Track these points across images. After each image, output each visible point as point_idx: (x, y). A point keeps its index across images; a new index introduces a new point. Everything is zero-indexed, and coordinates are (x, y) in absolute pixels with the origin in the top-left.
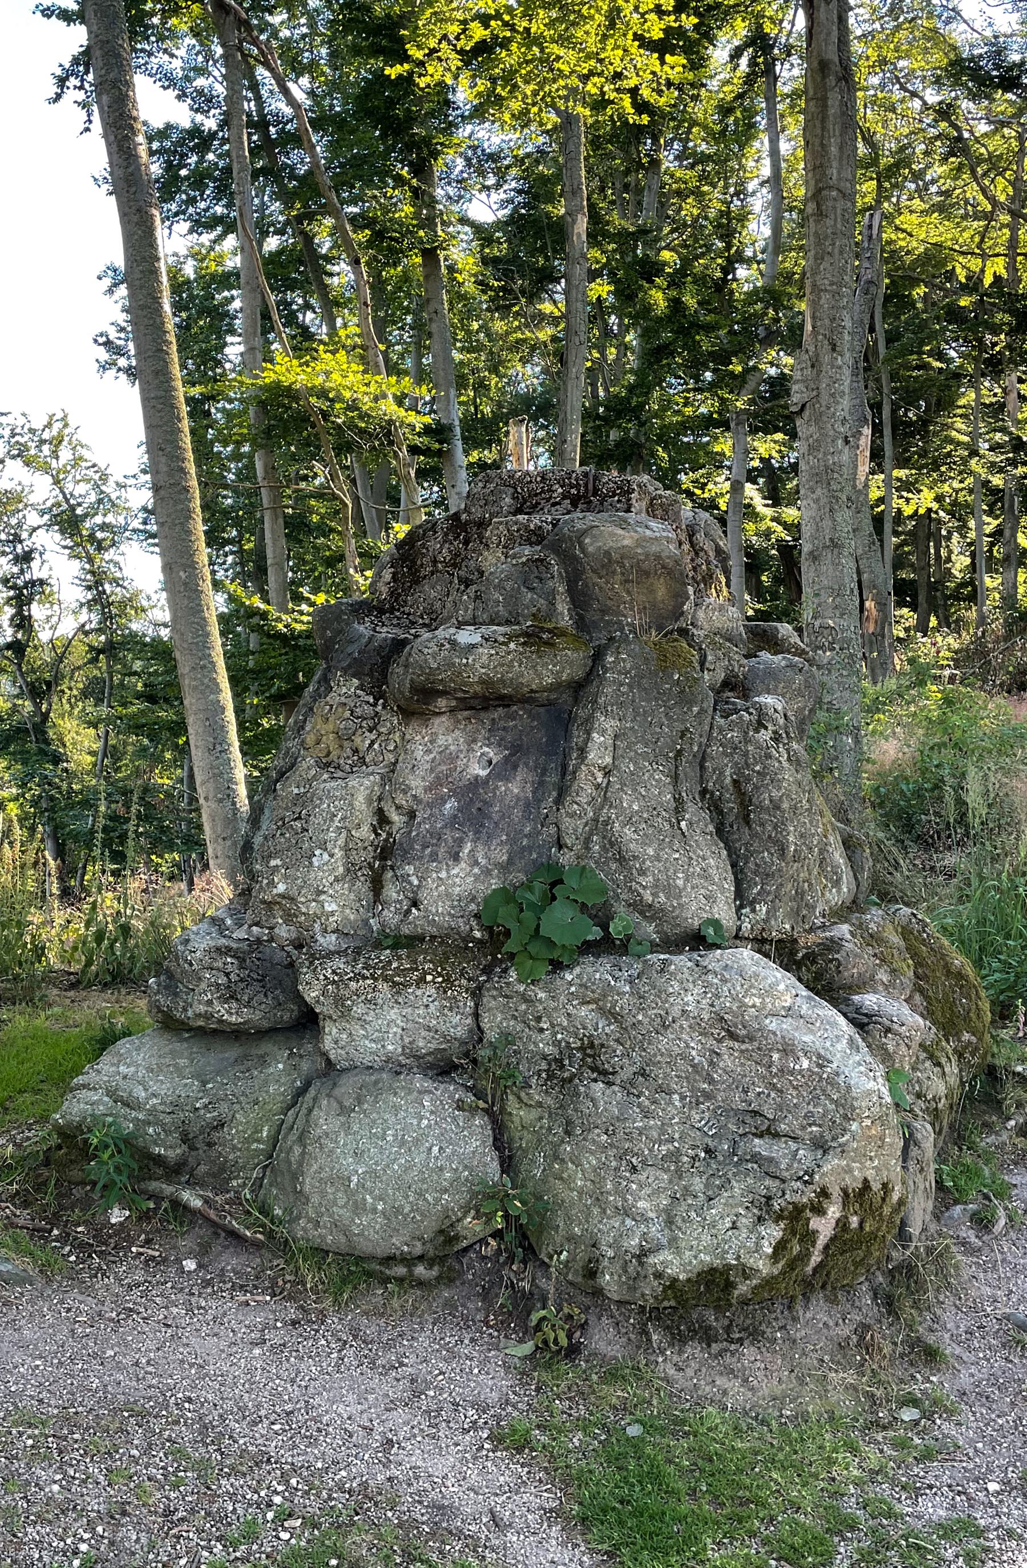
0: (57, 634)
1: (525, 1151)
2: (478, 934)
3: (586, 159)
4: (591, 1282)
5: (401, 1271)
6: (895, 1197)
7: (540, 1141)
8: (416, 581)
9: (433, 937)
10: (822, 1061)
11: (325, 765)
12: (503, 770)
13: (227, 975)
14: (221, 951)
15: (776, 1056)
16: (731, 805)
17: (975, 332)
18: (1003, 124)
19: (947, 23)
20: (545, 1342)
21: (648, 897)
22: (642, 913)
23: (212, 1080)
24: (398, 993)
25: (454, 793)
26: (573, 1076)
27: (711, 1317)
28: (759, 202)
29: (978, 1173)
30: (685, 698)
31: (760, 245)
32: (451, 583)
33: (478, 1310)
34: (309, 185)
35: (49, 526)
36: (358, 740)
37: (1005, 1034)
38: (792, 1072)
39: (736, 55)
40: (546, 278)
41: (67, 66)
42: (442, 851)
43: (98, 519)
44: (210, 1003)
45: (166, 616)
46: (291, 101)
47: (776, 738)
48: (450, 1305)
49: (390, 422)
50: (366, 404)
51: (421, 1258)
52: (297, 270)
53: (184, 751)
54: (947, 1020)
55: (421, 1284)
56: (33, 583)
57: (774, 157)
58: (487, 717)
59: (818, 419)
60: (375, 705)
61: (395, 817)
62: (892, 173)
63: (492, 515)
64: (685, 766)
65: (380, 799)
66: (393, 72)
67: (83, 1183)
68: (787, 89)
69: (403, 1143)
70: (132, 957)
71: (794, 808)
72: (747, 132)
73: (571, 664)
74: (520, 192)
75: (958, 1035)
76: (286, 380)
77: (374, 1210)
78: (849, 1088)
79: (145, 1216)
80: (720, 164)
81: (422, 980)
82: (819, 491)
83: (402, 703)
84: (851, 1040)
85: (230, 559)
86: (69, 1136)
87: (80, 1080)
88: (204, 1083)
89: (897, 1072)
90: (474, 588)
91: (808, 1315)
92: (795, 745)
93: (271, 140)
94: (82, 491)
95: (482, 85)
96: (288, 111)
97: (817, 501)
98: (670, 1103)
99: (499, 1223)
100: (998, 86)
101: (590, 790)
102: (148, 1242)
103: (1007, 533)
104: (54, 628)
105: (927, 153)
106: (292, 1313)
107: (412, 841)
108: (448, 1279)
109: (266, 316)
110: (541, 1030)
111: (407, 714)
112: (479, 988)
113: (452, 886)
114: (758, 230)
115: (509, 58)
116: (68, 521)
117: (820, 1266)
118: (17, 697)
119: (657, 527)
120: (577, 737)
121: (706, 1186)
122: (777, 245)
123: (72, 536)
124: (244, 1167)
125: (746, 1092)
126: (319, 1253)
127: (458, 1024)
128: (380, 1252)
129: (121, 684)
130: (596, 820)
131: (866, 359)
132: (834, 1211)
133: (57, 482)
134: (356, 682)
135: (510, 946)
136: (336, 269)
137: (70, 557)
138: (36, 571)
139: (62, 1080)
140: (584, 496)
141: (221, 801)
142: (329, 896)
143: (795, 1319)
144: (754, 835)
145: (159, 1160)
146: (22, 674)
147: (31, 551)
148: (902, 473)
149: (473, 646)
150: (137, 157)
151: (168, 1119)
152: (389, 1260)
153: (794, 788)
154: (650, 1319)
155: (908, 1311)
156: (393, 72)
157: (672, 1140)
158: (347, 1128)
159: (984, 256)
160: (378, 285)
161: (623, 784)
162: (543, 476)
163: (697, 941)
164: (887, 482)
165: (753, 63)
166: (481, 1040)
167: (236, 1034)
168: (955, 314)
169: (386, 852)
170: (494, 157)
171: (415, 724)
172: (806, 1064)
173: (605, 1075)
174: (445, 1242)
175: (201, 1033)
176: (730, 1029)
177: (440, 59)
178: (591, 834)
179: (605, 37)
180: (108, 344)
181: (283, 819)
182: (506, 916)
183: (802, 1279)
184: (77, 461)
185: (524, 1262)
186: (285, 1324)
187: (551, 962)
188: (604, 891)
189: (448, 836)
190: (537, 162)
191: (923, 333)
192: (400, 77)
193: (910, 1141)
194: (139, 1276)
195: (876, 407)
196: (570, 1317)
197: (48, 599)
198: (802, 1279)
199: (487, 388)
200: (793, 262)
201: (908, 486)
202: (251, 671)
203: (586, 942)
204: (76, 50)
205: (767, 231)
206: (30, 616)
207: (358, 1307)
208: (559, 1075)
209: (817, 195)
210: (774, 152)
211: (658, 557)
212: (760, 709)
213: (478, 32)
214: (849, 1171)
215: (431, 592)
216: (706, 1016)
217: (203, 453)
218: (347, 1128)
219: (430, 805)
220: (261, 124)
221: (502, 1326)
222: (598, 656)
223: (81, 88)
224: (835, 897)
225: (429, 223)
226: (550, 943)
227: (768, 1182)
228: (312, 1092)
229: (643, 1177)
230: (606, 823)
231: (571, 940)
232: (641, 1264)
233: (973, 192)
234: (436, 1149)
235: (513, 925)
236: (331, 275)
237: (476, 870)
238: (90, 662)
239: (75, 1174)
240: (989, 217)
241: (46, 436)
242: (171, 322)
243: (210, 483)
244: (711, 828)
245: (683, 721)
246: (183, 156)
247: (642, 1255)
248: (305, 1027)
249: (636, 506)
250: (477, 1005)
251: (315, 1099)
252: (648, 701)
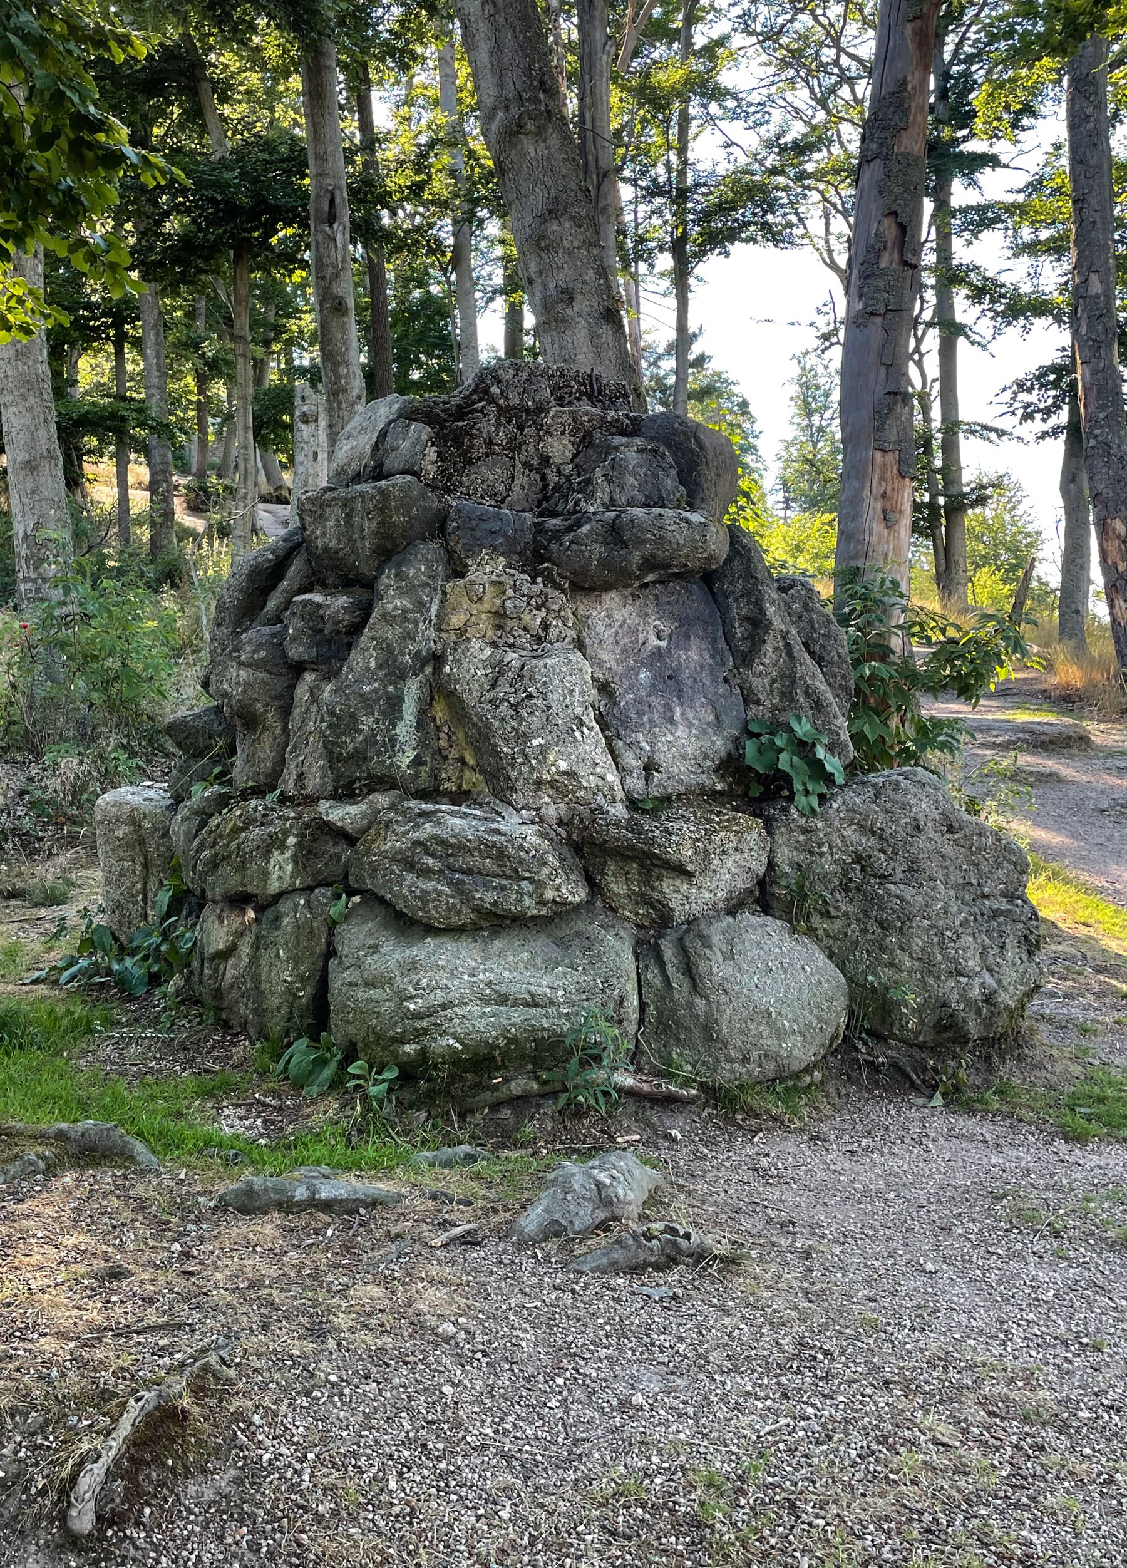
32: (514, 466)
82: (32, 400)
97: (30, 409)
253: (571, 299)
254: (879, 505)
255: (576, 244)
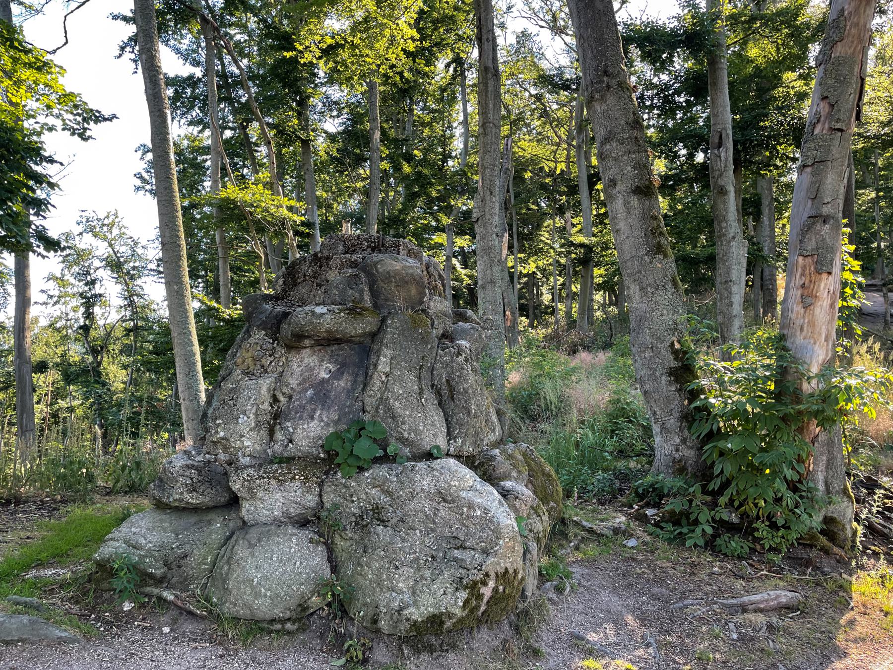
0: (108, 321)
1: (343, 562)
2: (322, 456)
3: (380, 106)
4: (375, 626)
5: (278, 626)
6: (520, 576)
7: (351, 557)
8: (295, 284)
9: (300, 458)
10: (486, 511)
11: (246, 373)
12: (336, 375)
13: (192, 479)
14: (188, 467)
15: (465, 509)
16: (445, 392)
17: (553, 195)
18: (564, 105)
19: (540, 59)
20: (351, 658)
21: (406, 435)
22: (403, 443)
23: (182, 533)
24: (281, 485)
25: (312, 386)
26: (368, 523)
27: (433, 640)
28: (459, 131)
29: (557, 567)
30: (424, 340)
31: (459, 151)
33: (318, 644)
34: (246, 108)
35: (105, 267)
36: (264, 361)
37: (569, 503)
38: (472, 517)
39: (448, 66)
40: (359, 160)
41: (126, 41)
42: (305, 415)
43: (132, 264)
44: (182, 493)
45: (167, 314)
46: (239, 67)
47: (466, 360)
48: (303, 642)
49: (284, 219)
50: (273, 210)
51: (289, 619)
52: (240, 148)
53: (172, 379)
54: (544, 496)
55: (289, 633)
56: (96, 296)
57: (464, 112)
58: (329, 349)
59: (485, 225)
60: (273, 343)
61: (282, 399)
62: (517, 122)
63: (333, 255)
64: (424, 373)
65: (274, 390)
66: (288, 55)
67: (110, 590)
68: (471, 83)
69: (281, 561)
70: (141, 478)
71: (474, 392)
72: (453, 99)
73: (371, 324)
74: (349, 120)
75: (548, 503)
76: (232, 197)
77: (266, 596)
78: (499, 523)
79: (143, 606)
80: (440, 115)
81: (293, 478)
82: (485, 258)
83: (287, 342)
84: (500, 501)
85: (201, 285)
86: (102, 566)
87: (110, 536)
88: (177, 535)
89: (521, 517)
90: (323, 288)
91: (479, 636)
92: (475, 363)
93: (227, 83)
94: (123, 250)
95: (331, 64)
96: (237, 72)
97: (484, 262)
98: (415, 534)
99: (329, 598)
100: (562, 88)
101: (379, 384)
102: (144, 619)
103: (567, 284)
104: (106, 319)
105: (531, 115)
106: (221, 651)
107: (290, 411)
108: (303, 629)
109: (224, 169)
110: (353, 502)
111: (289, 348)
112: (322, 482)
113: (309, 432)
114: (457, 145)
115: (344, 54)
116: (115, 265)
117: (485, 611)
118: (84, 354)
119: (411, 261)
120: (373, 359)
121: (432, 574)
122: (466, 152)
123: (118, 272)
124: (197, 578)
125: (451, 527)
126: (237, 619)
127: (311, 500)
128: (267, 617)
129: (141, 347)
130: (381, 398)
131: (505, 203)
132: (491, 584)
133: (111, 245)
134: (263, 332)
135: (338, 460)
136: (259, 149)
137: (116, 283)
138: (98, 289)
139: (99, 539)
140: (378, 247)
141: (191, 401)
142: (246, 437)
143: (473, 638)
144: (456, 406)
145: (151, 576)
146: (88, 342)
147: (95, 280)
148: (522, 255)
149: (323, 314)
150: (159, 85)
151: (157, 554)
152: (272, 621)
153: (474, 383)
154: (403, 642)
155: (526, 632)
156: (288, 55)
157: (415, 552)
158: (252, 554)
159: (556, 162)
160: (279, 155)
161: (395, 381)
162: (358, 237)
163: (429, 456)
164: (515, 259)
165: (455, 70)
166: (322, 507)
167: (195, 510)
168: (544, 187)
169: (276, 416)
170: (337, 103)
171: (293, 353)
172: (479, 513)
173: (383, 522)
174: (302, 611)
175: (177, 509)
176: (444, 497)
177: (310, 51)
178: (379, 405)
179: (388, 48)
180: (141, 177)
181: (224, 400)
182: (336, 446)
183: (477, 618)
184: (121, 235)
185: (342, 618)
186: (216, 657)
187: (359, 467)
188: (385, 432)
189: (308, 407)
190: (357, 107)
191: (531, 194)
192: (291, 57)
193: (526, 552)
194: (138, 637)
195: (510, 226)
196: (364, 645)
197: (104, 305)
198: (477, 618)
199: (332, 208)
200: (474, 159)
201: (524, 261)
202: (211, 337)
203: (376, 458)
204: (131, 34)
205: (462, 146)
206: (93, 313)
207: (255, 646)
208: (361, 523)
209: (483, 125)
210: (465, 110)
211: (412, 275)
212: (459, 347)
213: (329, 41)
214: (499, 564)
215: (302, 290)
216: (432, 491)
217: (189, 234)
218: (252, 554)
219: (300, 392)
220: (223, 76)
221: (330, 651)
222: (383, 321)
223: (133, 52)
224: (493, 437)
225: (305, 128)
226: (358, 458)
227: (461, 571)
228: (235, 537)
229: (401, 572)
230: (386, 399)
231: (368, 456)
232: (400, 614)
233: (551, 133)
234: (298, 563)
235: (339, 450)
236: (256, 151)
237: (322, 424)
238: (125, 336)
239: (105, 585)
240: (558, 145)
241: (106, 222)
242: (175, 169)
243: (193, 249)
244: (436, 402)
245: (423, 352)
246: (184, 88)
247: (400, 610)
248: (232, 505)
249: (402, 252)
250: (321, 490)
251: (236, 541)
252: (407, 342)
253: (615, 184)
254: (799, 293)
255: (620, 154)
